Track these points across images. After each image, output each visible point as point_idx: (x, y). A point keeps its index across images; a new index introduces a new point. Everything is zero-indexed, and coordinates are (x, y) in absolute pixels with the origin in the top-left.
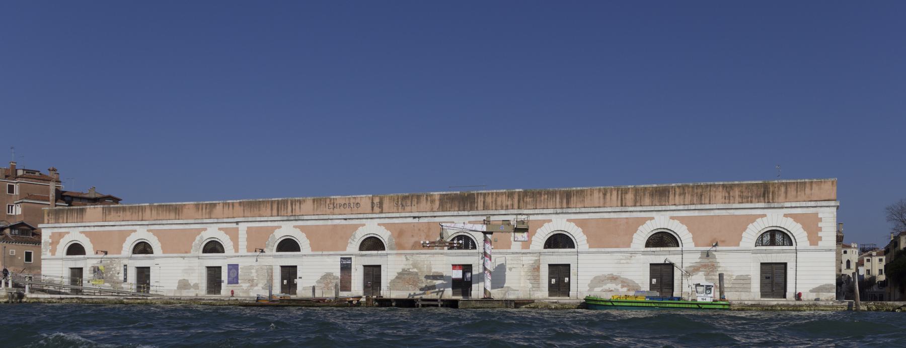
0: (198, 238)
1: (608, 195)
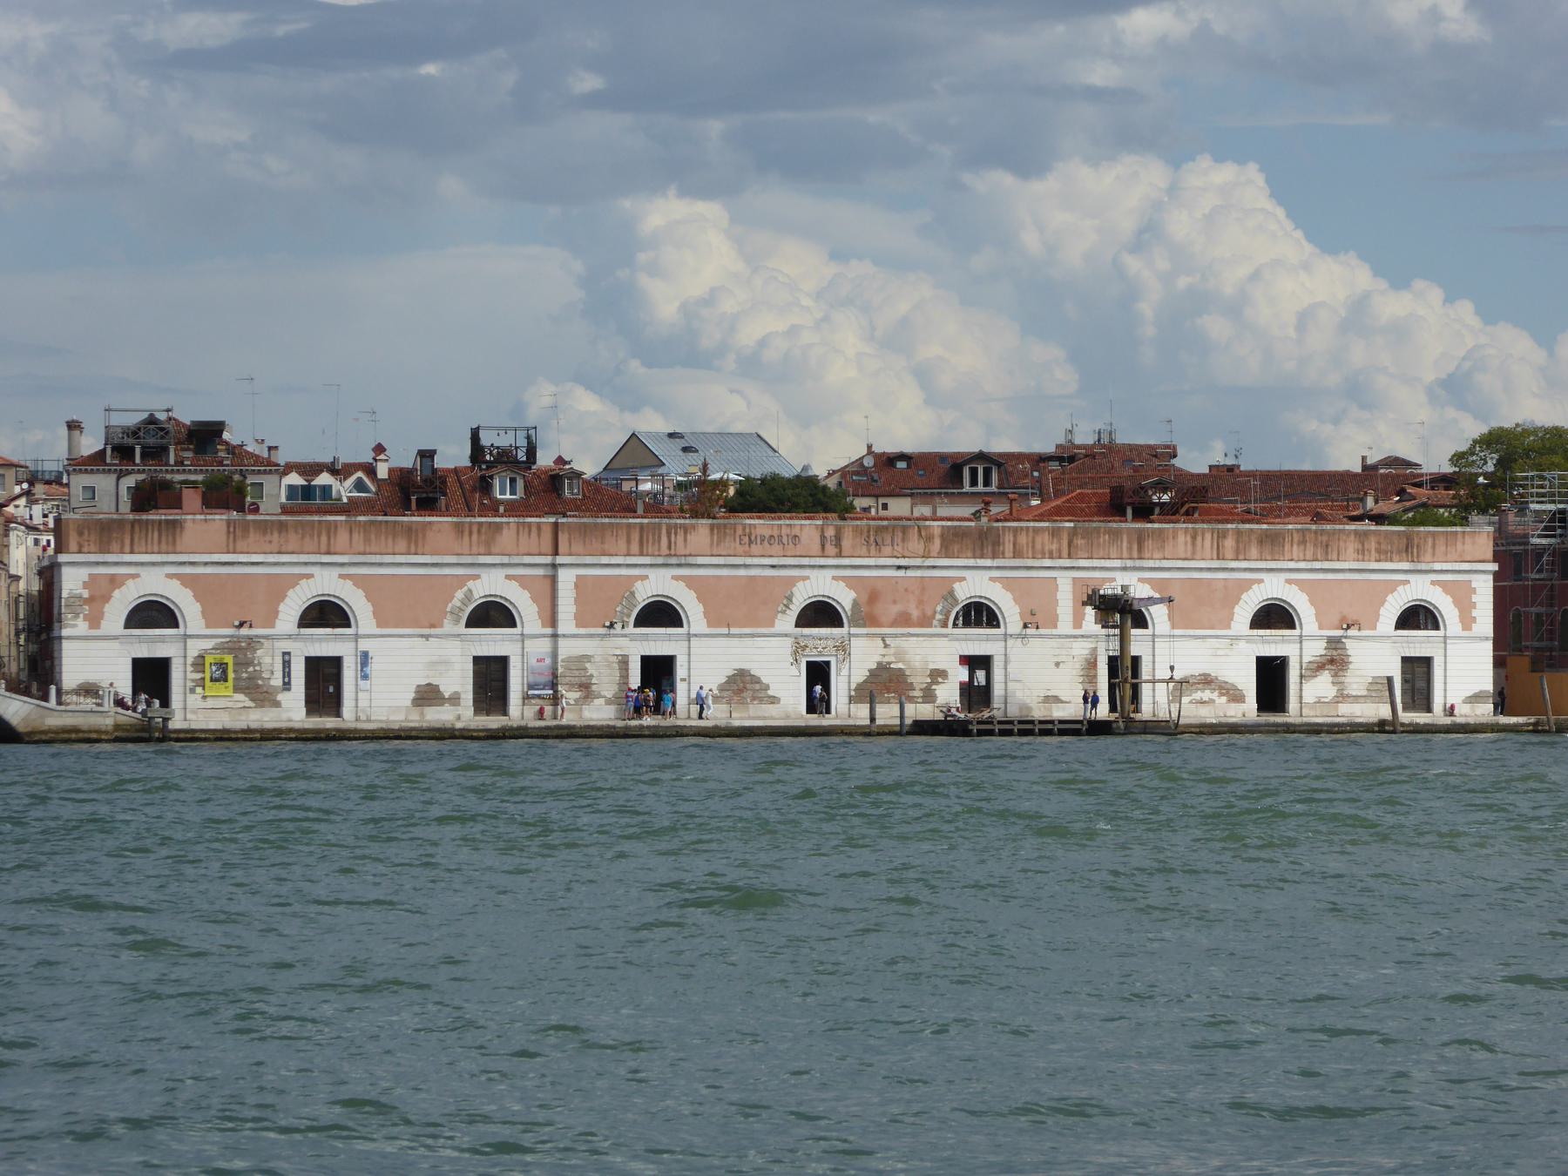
0: (460, 594)
1: (1199, 538)
